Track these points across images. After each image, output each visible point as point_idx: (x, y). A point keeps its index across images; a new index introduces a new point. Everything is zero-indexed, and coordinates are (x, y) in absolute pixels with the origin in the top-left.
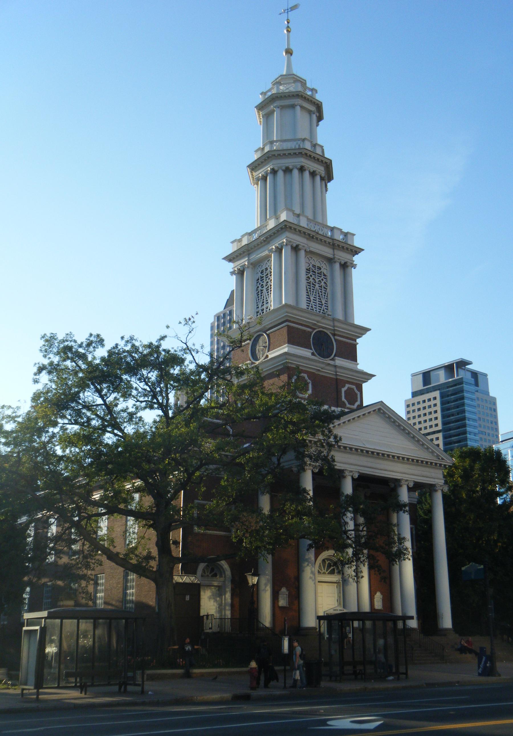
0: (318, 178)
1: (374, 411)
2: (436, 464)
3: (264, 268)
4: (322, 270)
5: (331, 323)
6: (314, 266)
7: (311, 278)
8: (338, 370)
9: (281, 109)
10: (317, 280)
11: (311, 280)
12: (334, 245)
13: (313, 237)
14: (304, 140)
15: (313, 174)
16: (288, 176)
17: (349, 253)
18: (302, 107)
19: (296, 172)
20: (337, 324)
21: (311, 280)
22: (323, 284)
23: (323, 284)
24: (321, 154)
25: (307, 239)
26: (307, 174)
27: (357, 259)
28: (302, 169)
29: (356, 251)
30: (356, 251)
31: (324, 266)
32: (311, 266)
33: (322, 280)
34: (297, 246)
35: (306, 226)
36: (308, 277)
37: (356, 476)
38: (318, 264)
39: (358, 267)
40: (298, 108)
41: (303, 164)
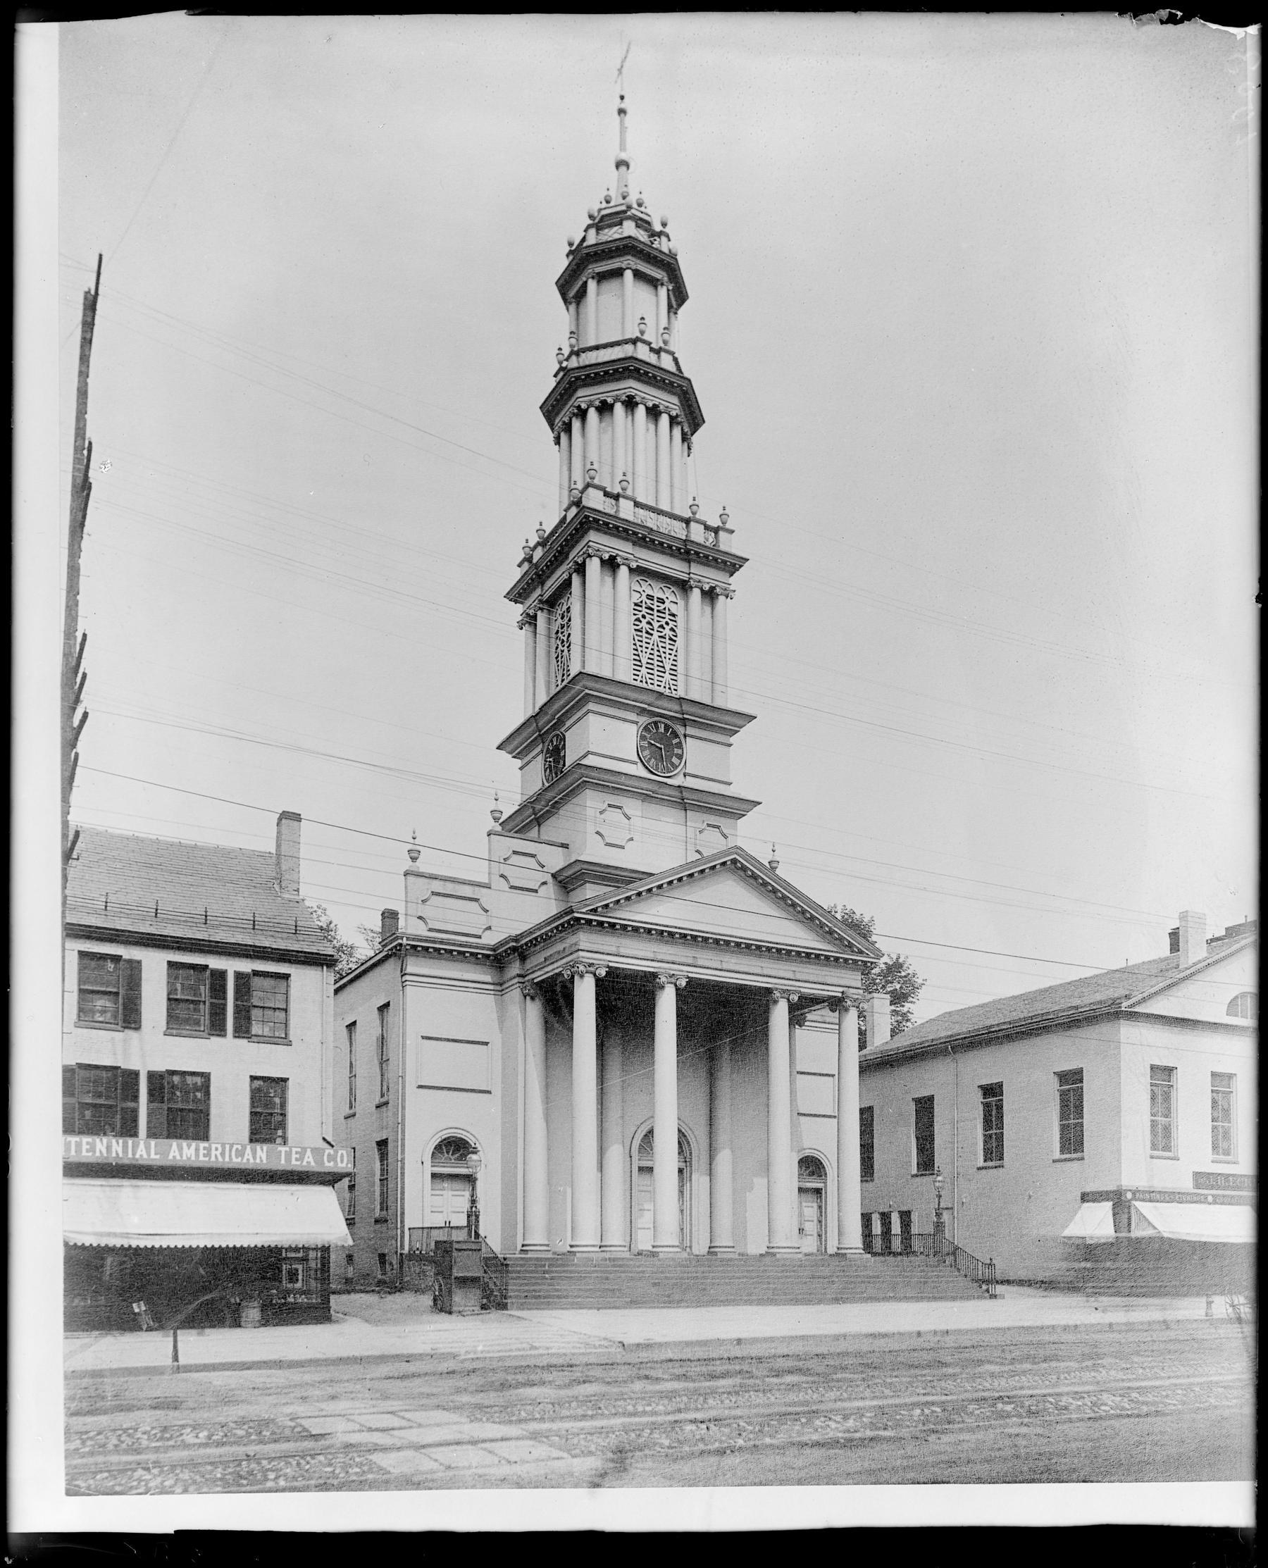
0: (664, 419)
1: (724, 864)
2: (837, 959)
3: (565, 608)
4: (667, 604)
5: (677, 708)
6: (650, 597)
7: (644, 621)
8: (685, 794)
9: (599, 282)
10: (656, 625)
11: (644, 624)
12: (688, 552)
13: (644, 538)
14: (634, 341)
15: (654, 413)
16: (607, 418)
17: (718, 569)
18: (638, 275)
19: (619, 408)
20: (686, 707)
21: (644, 624)
22: (667, 631)
23: (667, 631)
24: (673, 369)
25: (634, 544)
26: (641, 411)
27: (736, 581)
28: (630, 404)
29: (732, 565)
30: (732, 565)
31: (672, 598)
32: (644, 598)
33: (644, 617)
34: (712, 589)
35: (631, 518)
36: (638, 620)
37: (602, 972)
38: (657, 594)
39: (736, 596)
40: (628, 275)
41: (633, 392)
